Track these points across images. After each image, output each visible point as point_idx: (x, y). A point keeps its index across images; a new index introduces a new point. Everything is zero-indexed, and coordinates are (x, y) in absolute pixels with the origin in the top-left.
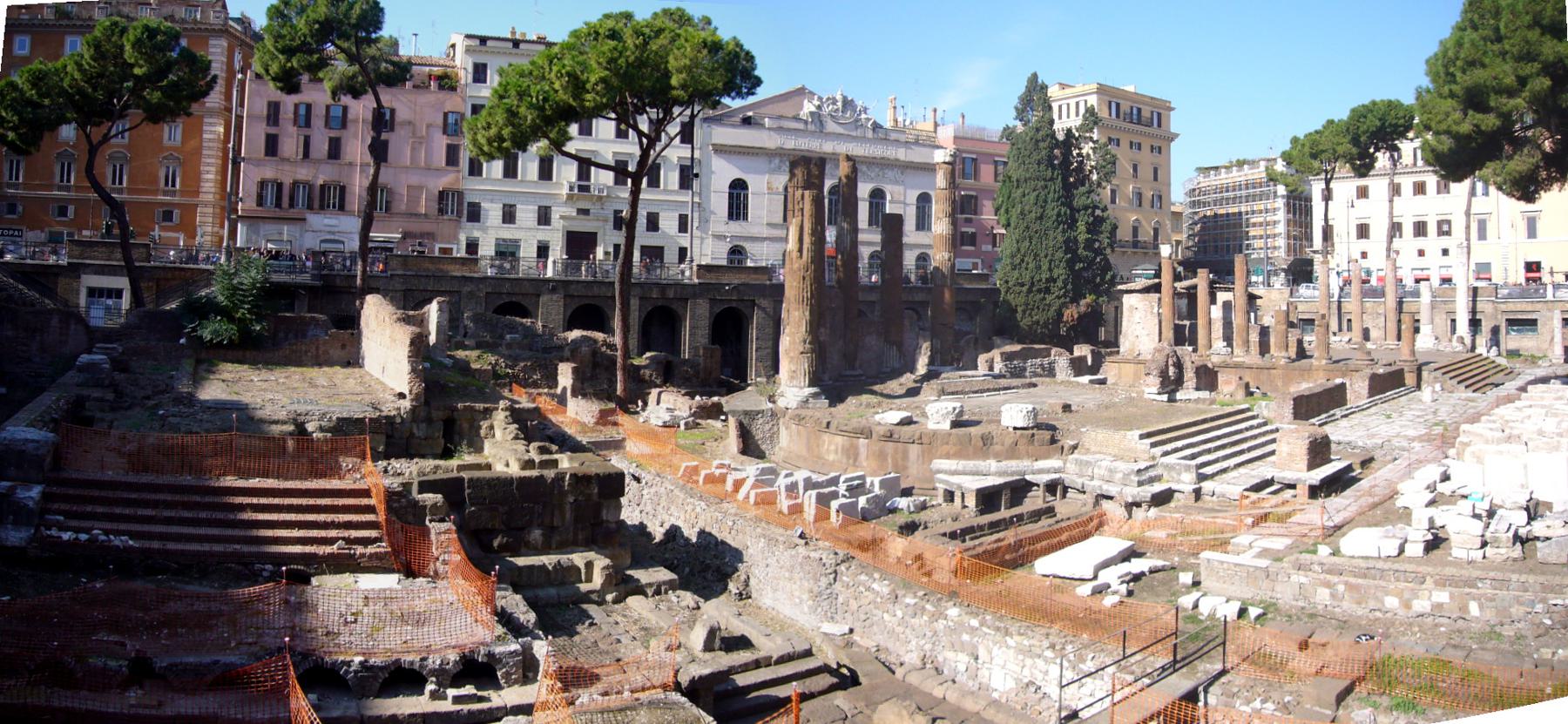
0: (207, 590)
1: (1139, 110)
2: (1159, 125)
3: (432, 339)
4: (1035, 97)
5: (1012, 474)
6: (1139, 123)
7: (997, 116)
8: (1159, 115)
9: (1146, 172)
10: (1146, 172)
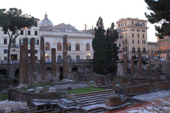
0: (111, 89)
1: (139, 23)
2: (144, 26)
3: (154, 14)
4: (100, 22)
5: (47, 102)
6: (139, 25)
7: (92, 25)
8: (144, 23)
9: (141, 36)
10: (141, 36)
